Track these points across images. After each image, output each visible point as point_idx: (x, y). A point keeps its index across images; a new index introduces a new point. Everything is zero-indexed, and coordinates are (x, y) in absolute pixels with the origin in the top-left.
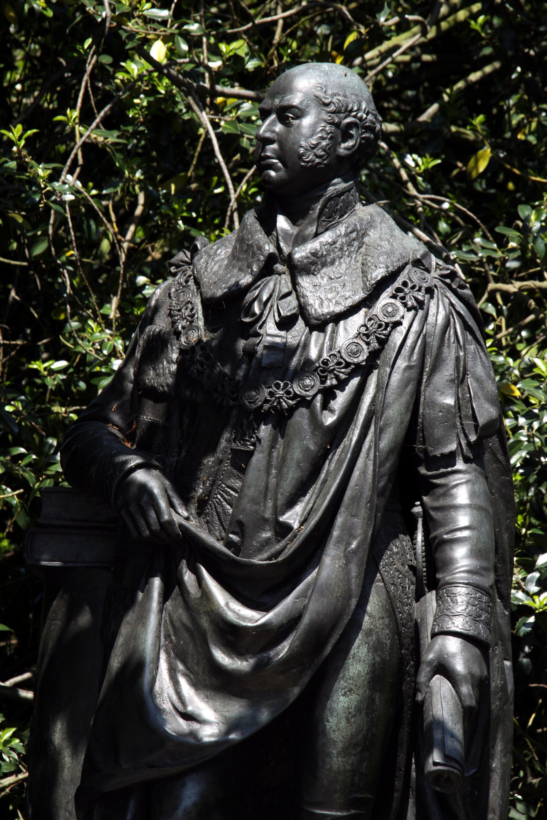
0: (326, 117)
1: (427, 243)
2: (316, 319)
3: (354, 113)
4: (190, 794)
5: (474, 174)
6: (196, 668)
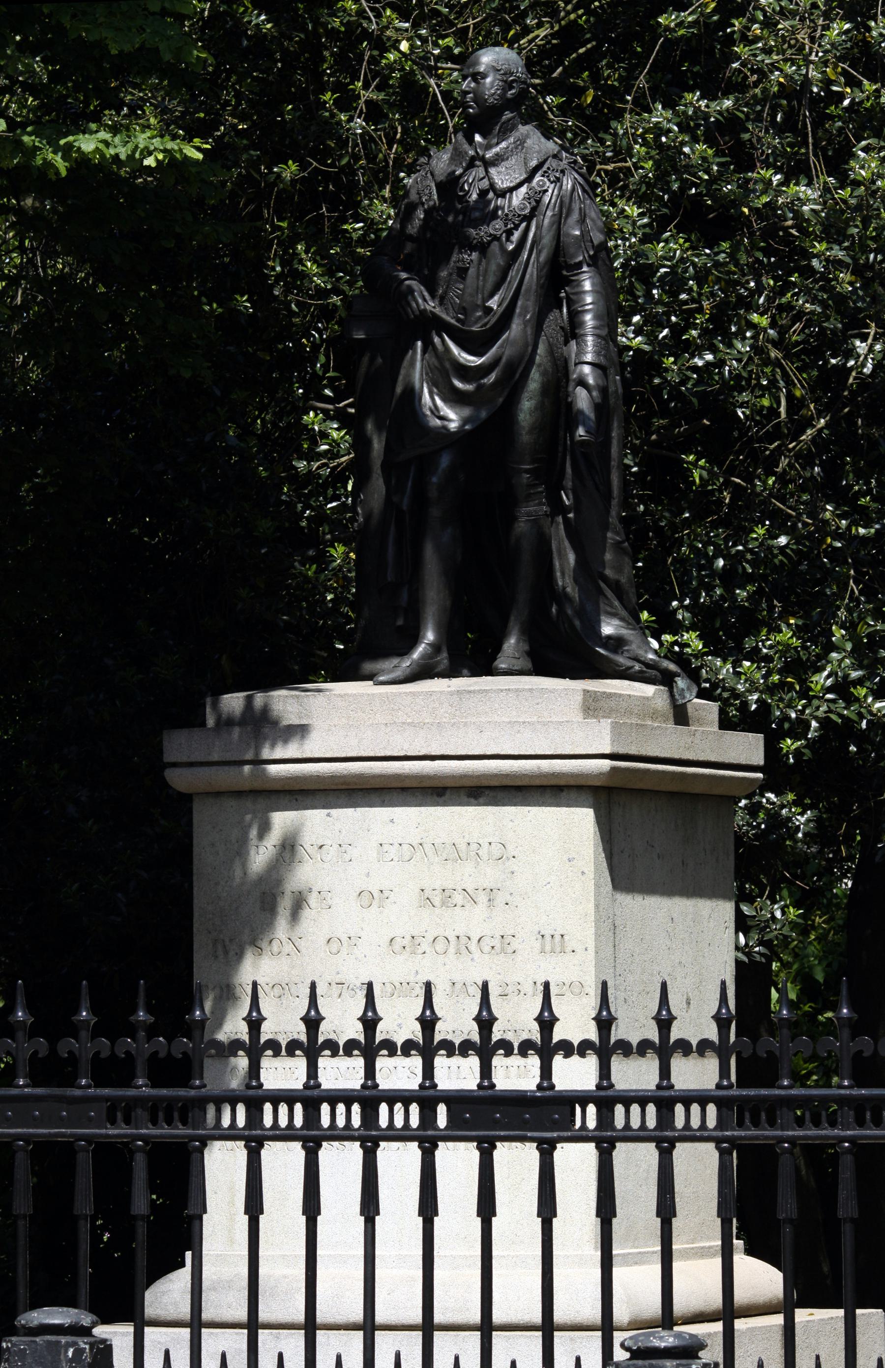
0: (499, 77)
1: (560, 145)
4: (445, 461)
5: (585, 105)
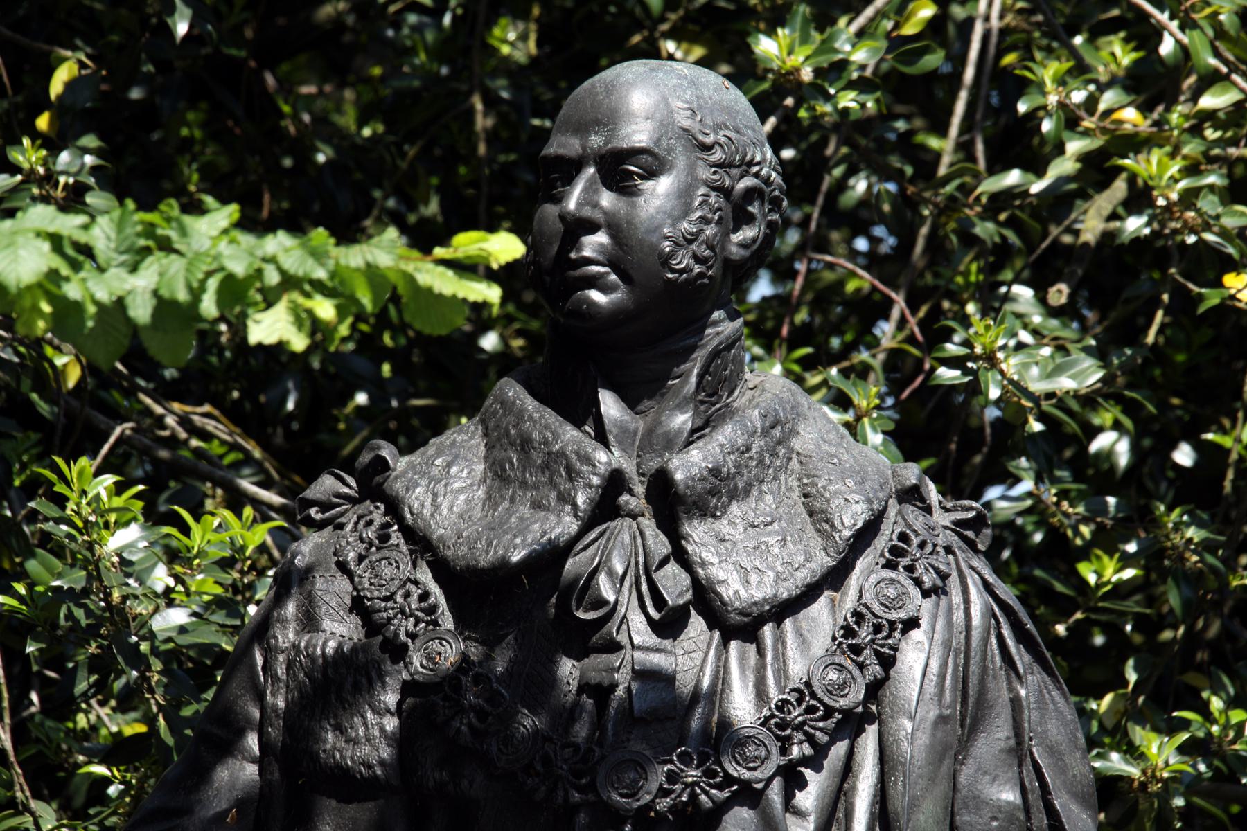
0: (705, 173)
2: (742, 613)
3: (756, 169)
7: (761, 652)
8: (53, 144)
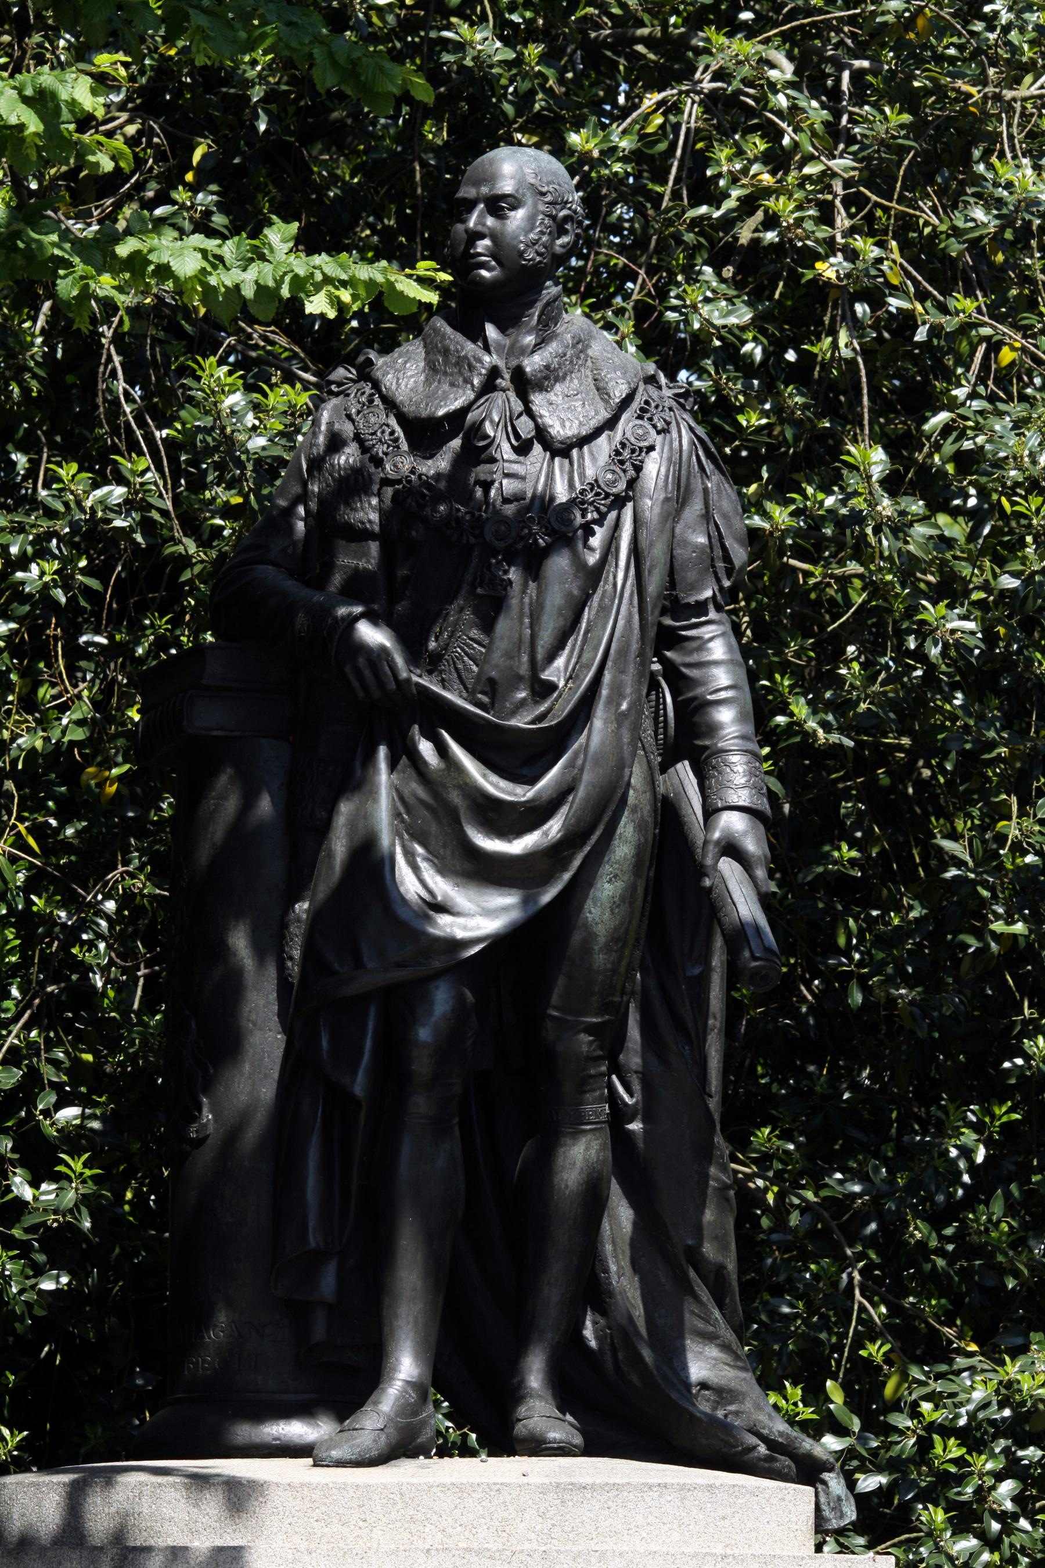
0: (542, 207)
2: (561, 442)
4: (442, 999)
6: (441, 851)
7: (571, 463)
8: (194, 189)
